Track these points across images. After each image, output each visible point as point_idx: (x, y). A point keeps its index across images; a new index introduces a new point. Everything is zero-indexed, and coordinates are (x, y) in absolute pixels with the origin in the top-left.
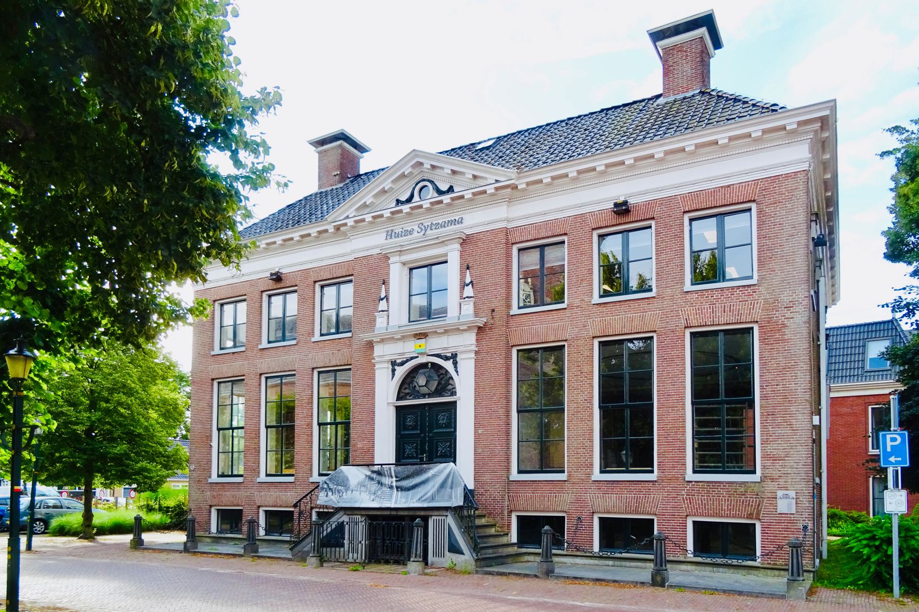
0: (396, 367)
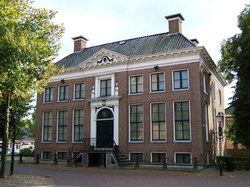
0: (97, 109)
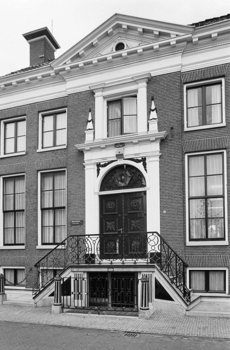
0: (100, 168)
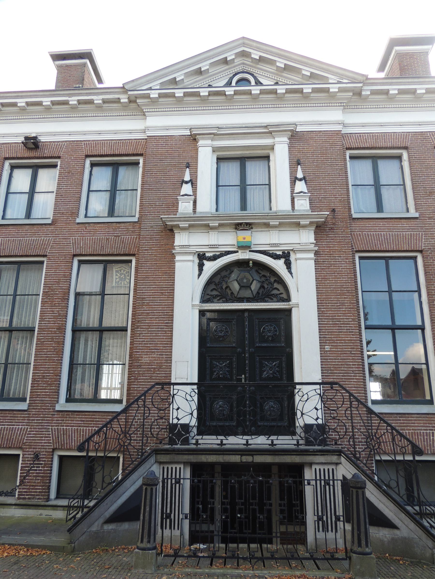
0: (205, 262)
